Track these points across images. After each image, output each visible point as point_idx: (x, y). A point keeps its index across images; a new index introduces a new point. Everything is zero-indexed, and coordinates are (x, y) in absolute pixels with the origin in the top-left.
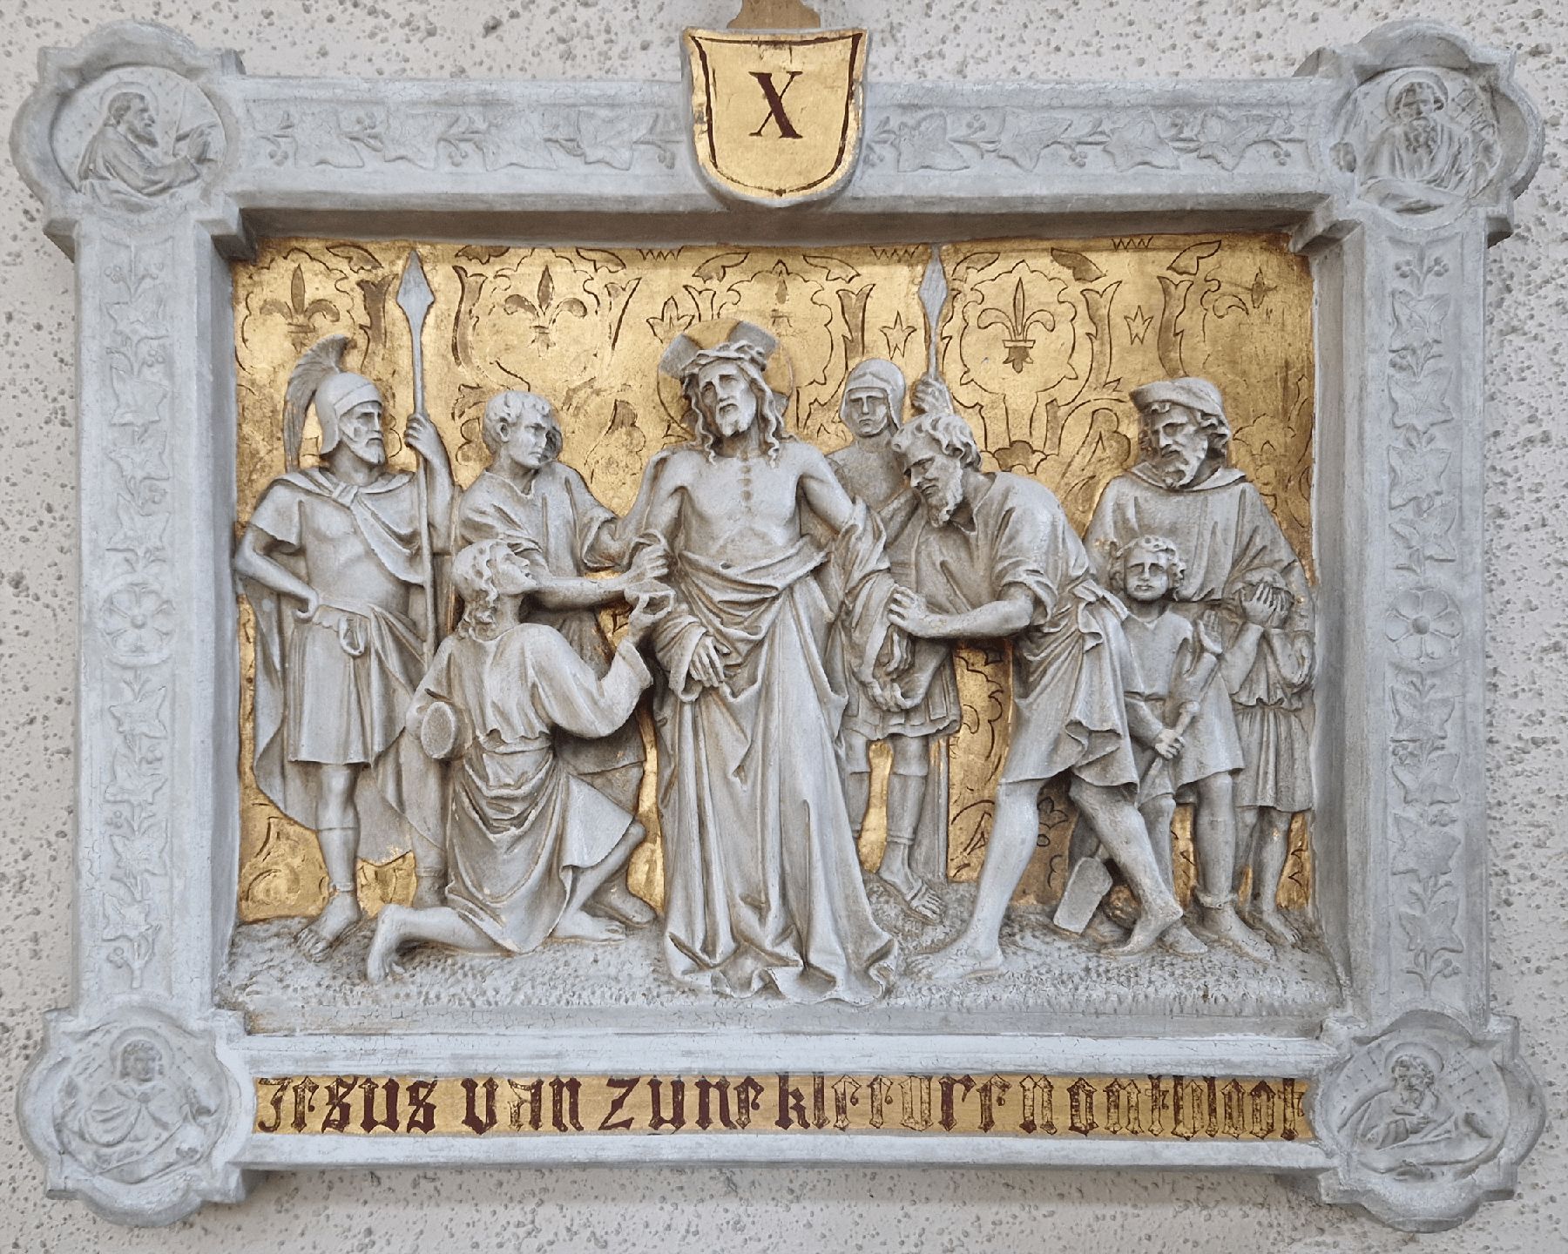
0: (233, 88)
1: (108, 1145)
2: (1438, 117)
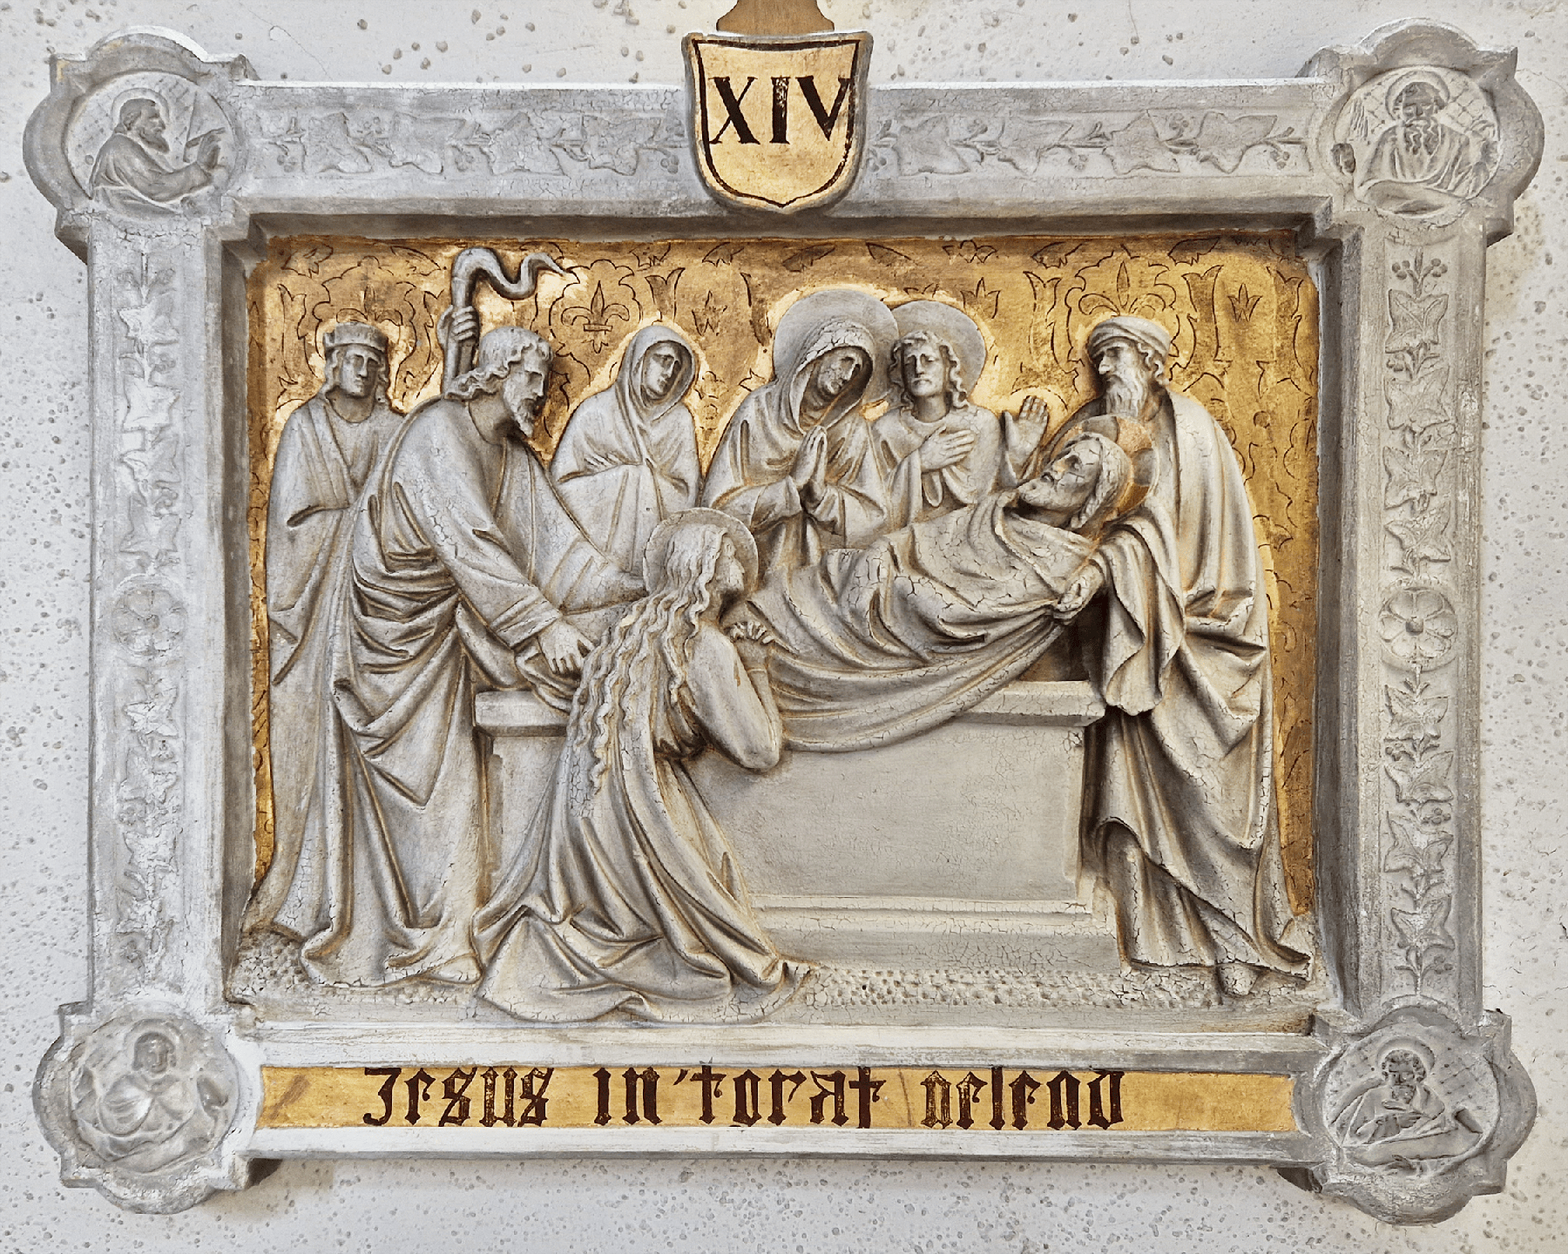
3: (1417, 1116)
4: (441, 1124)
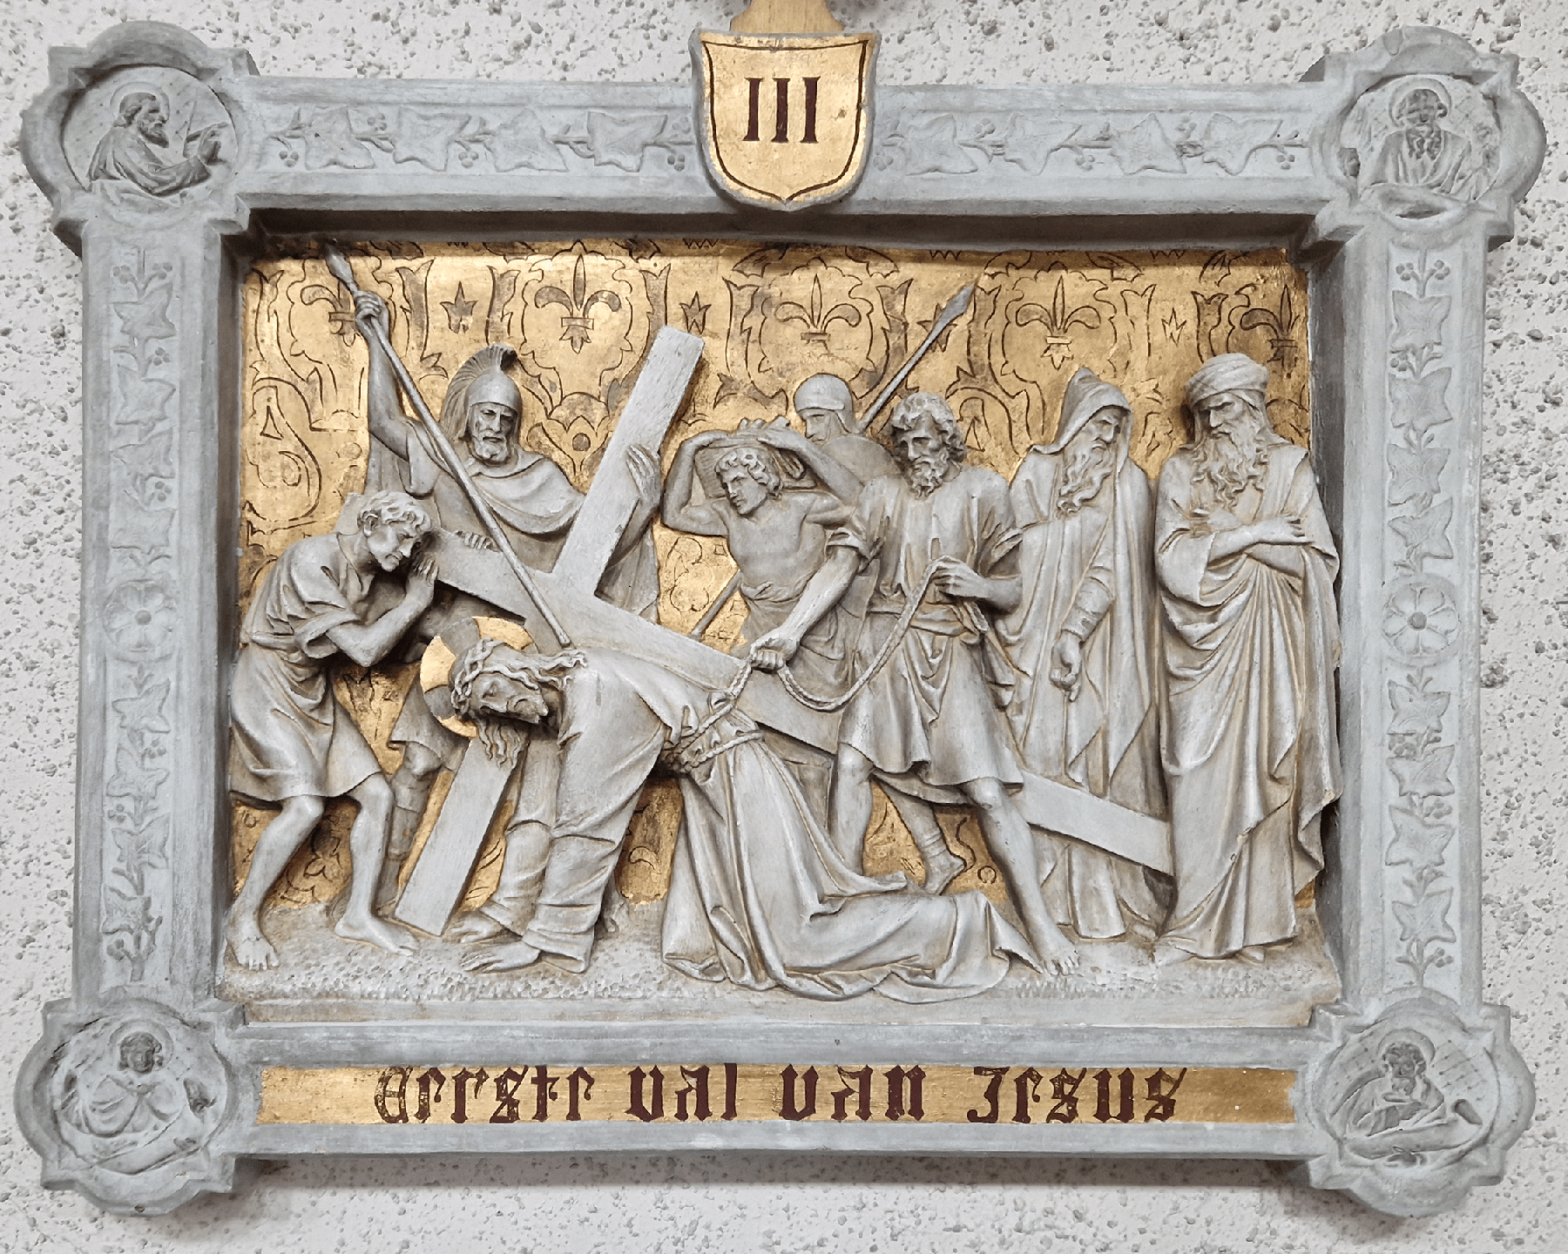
3: (1417, 1106)
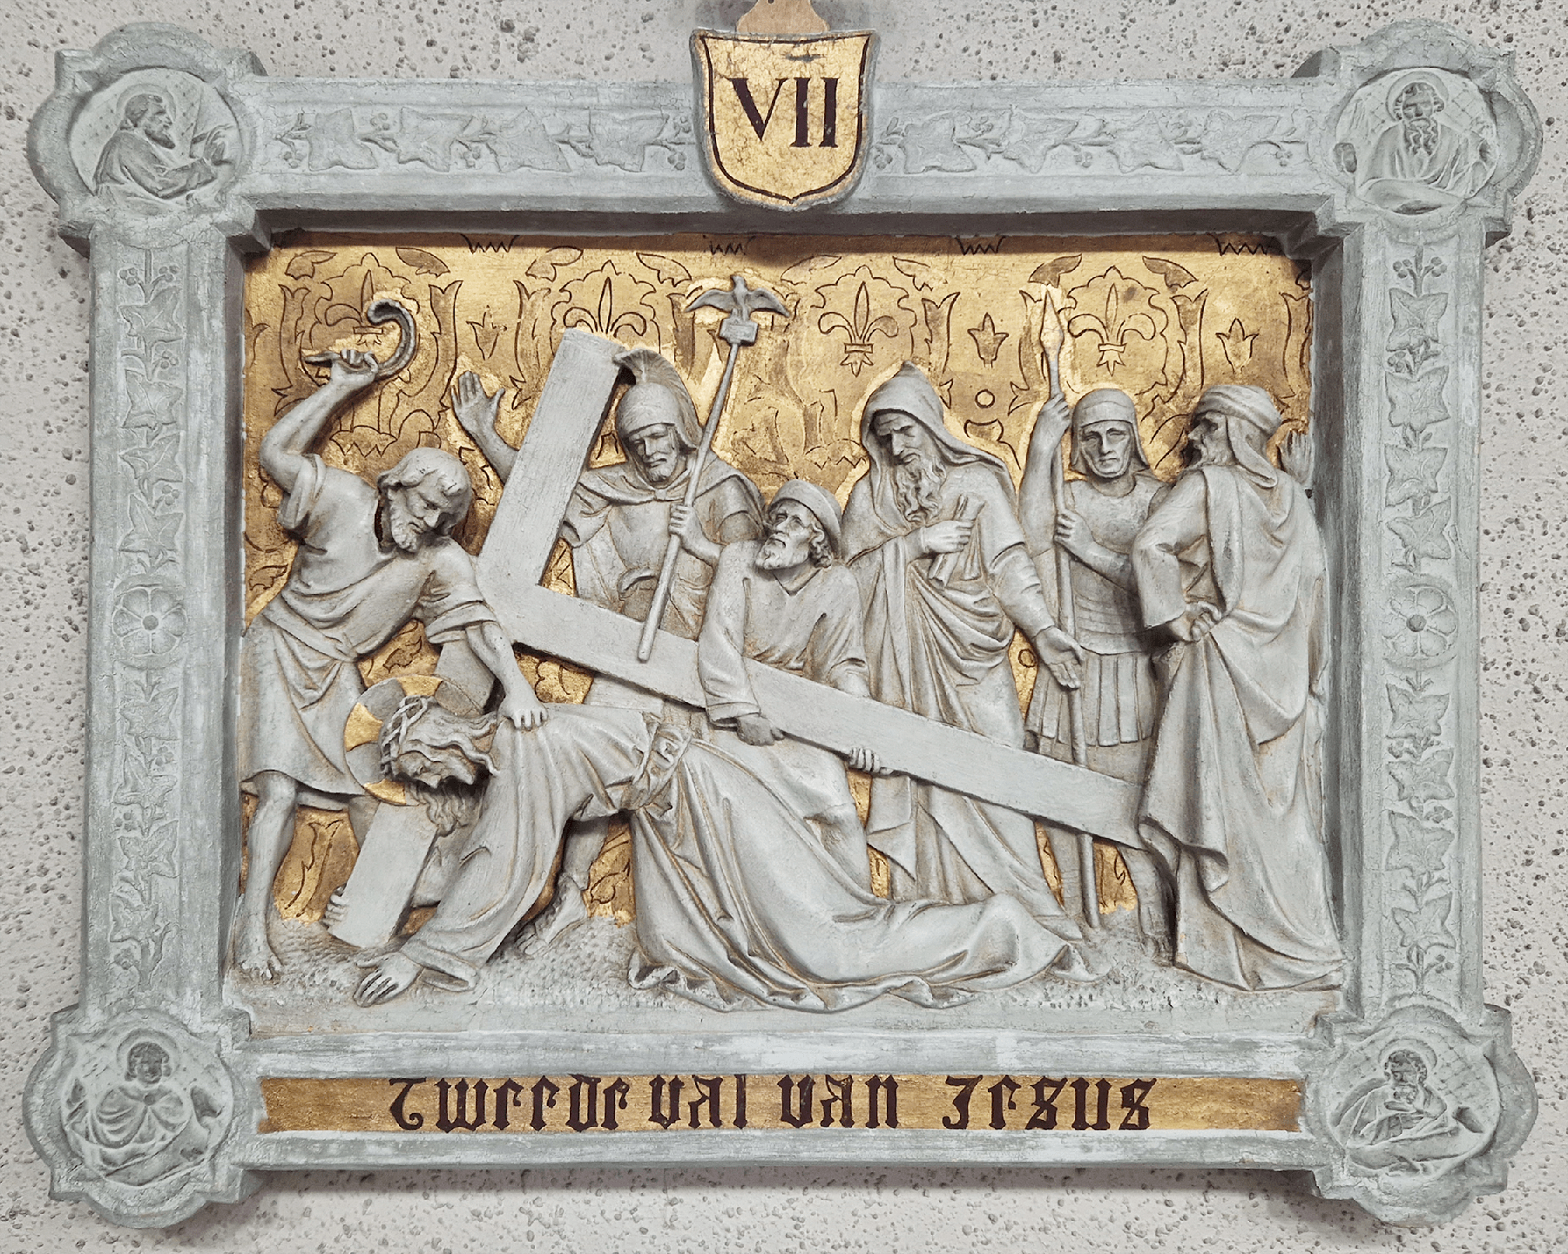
0: (252, 94)
1: (117, 1145)
2: (1440, 118)
4: (1029, 1127)
